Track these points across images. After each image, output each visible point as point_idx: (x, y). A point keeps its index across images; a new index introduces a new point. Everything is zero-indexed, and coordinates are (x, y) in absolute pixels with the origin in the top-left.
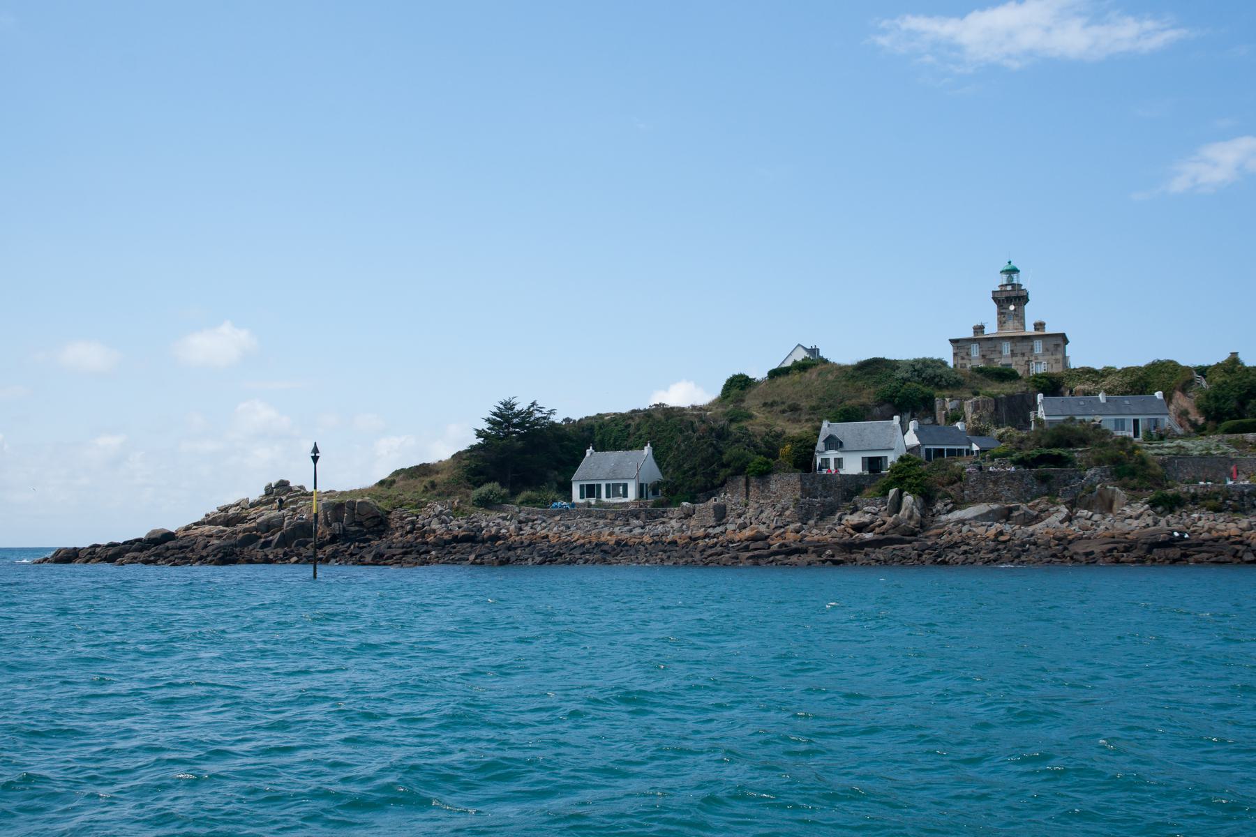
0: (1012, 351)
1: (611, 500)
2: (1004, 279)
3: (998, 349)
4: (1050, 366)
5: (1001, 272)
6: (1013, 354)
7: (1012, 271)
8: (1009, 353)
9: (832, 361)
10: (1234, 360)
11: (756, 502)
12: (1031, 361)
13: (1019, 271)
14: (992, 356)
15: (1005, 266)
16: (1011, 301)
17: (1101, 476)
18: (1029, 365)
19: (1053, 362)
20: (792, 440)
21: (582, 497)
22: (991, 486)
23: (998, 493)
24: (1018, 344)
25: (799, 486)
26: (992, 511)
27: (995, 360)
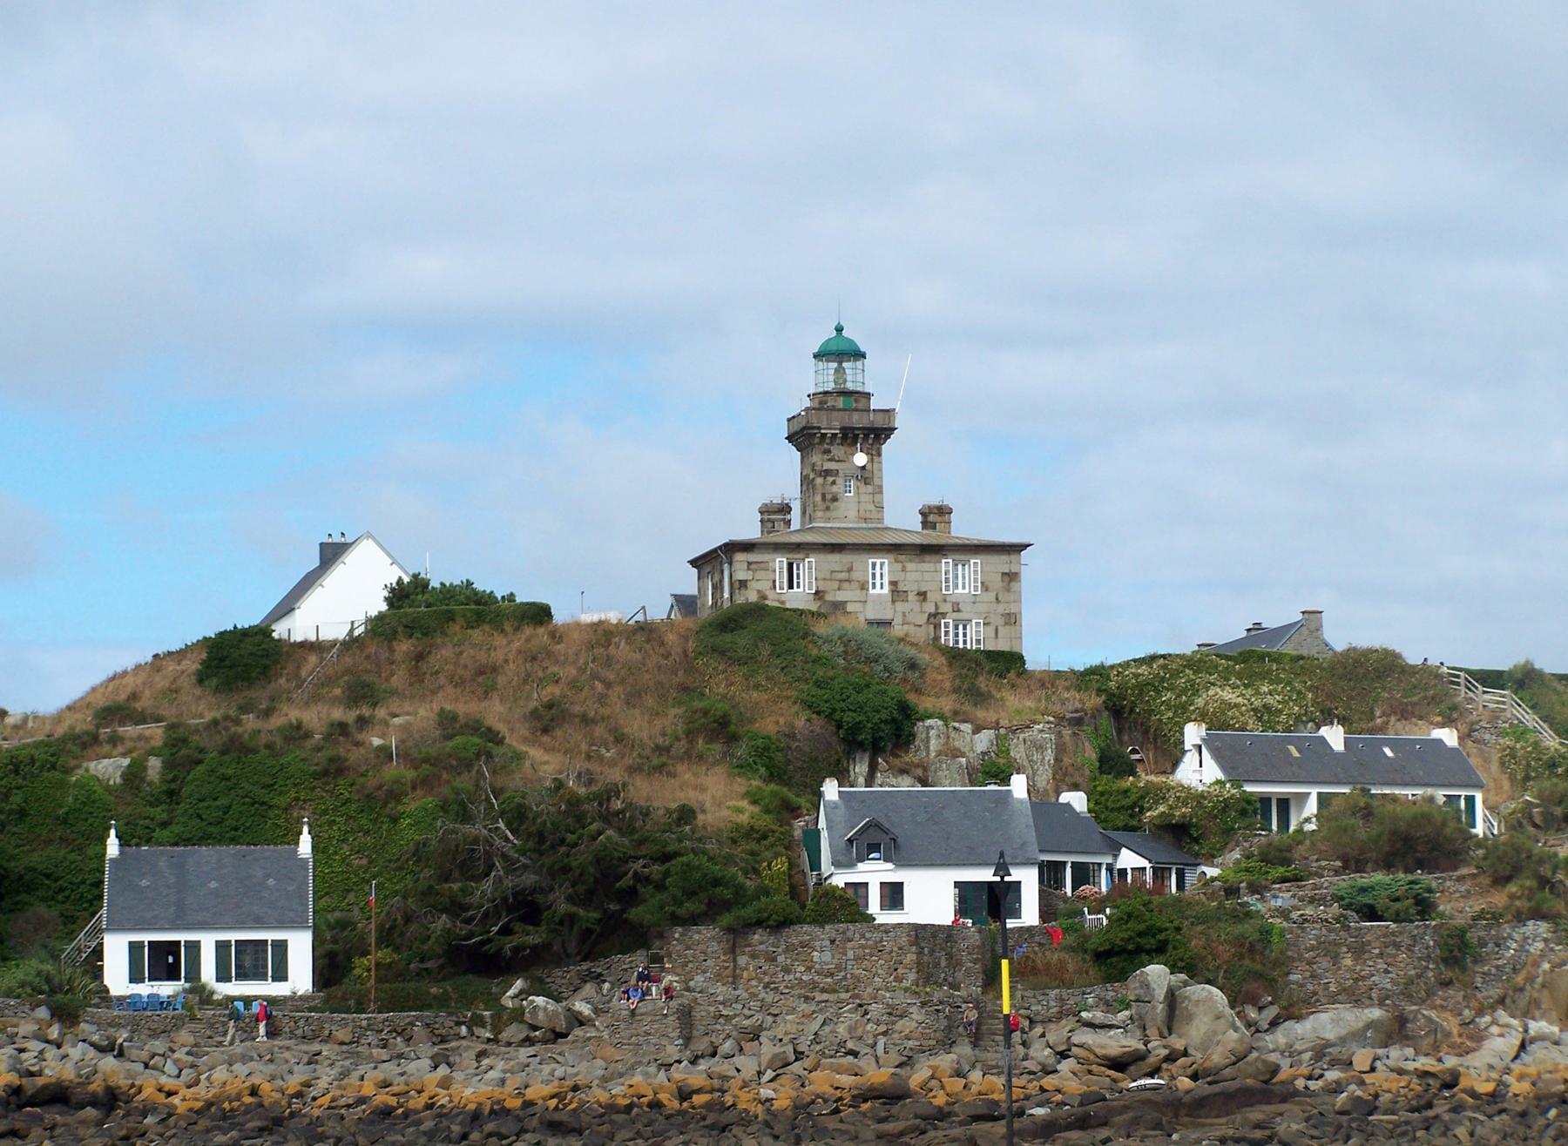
0: (893, 583)
1: (144, 989)
2: (824, 377)
3: (855, 575)
4: (991, 630)
5: (816, 356)
6: (897, 592)
7: (841, 352)
8: (886, 590)
9: (1413, 658)
10: (469, 583)
11: (807, 999)
12: (944, 615)
13: (863, 356)
14: (840, 596)
15: (822, 335)
16: (856, 437)
17: (1546, 940)
18: (937, 626)
19: (1001, 621)
20: (675, 810)
21: (135, 977)
22: (1348, 962)
23: (1363, 978)
24: (910, 566)
25: (910, 958)
26: (1370, 1025)
27: (850, 608)
